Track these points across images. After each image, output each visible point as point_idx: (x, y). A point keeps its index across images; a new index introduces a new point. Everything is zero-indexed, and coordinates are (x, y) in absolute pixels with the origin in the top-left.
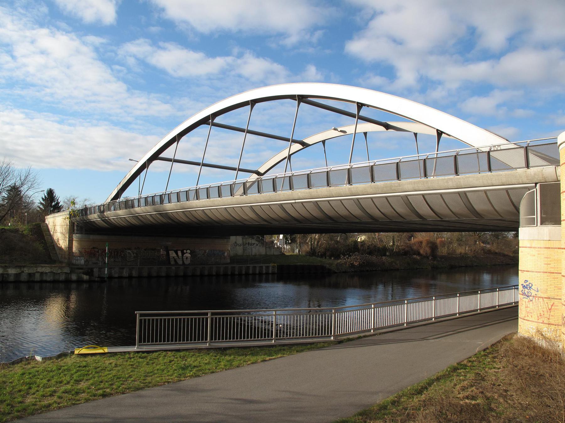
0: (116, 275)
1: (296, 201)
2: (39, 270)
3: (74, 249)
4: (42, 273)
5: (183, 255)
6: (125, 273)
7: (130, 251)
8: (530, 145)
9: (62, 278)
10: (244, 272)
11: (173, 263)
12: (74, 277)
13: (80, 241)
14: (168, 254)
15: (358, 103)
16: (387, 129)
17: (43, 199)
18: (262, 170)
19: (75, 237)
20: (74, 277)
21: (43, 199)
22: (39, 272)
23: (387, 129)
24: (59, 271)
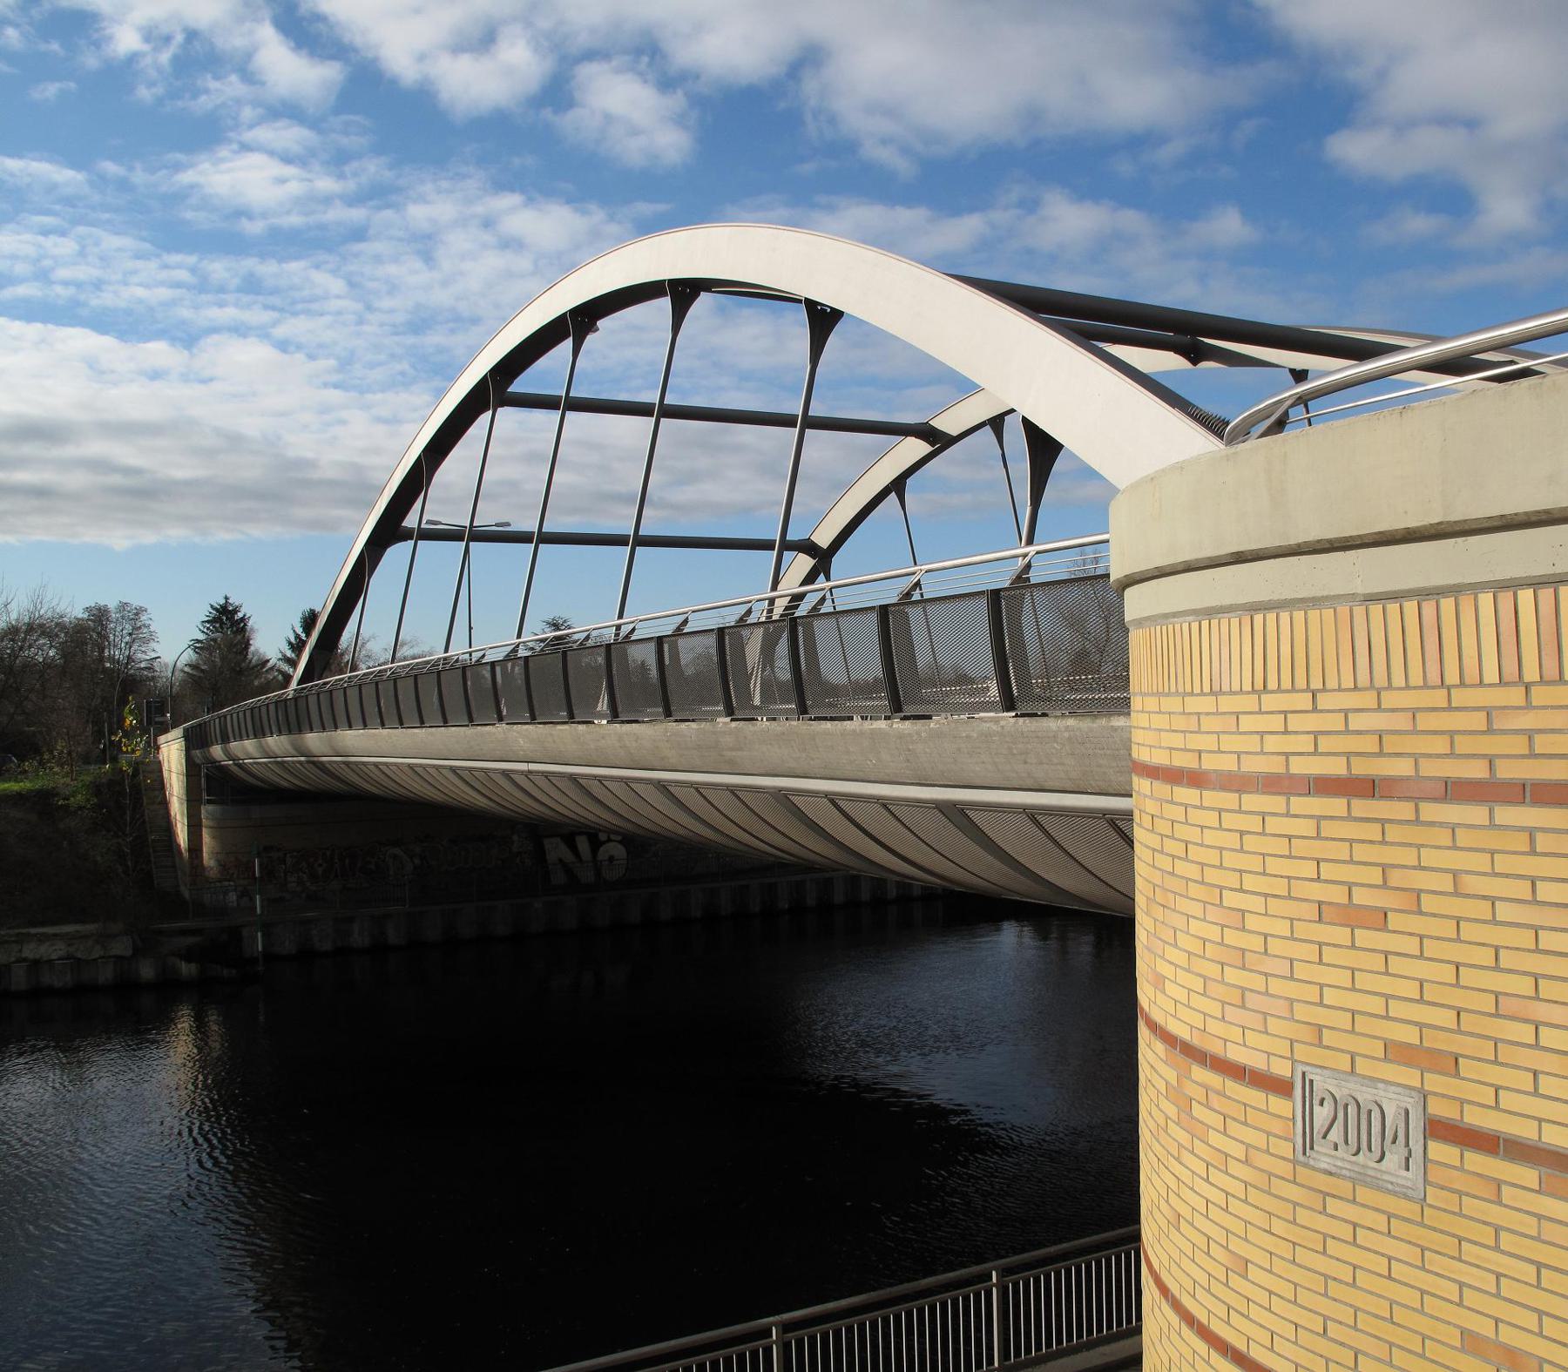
0: (327, 946)
1: (533, 767)
2: (30, 951)
3: (207, 858)
4: (36, 964)
5: (595, 851)
6: (359, 937)
7: (397, 851)
8: (1035, 577)
9: (106, 975)
10: (811, 901)
11: (559, 878)
12: (147, 971)
13: (219, 829)
14: (540, 854)
15: (811, 305)
16: (1195, 362)
17: (290, 643)
18: (823, 539)
19: (206, 811)
20: (147, 971)
21: (290, 643)
22: (25, 960)
23: (1195, 362)
24: (97, 953)
